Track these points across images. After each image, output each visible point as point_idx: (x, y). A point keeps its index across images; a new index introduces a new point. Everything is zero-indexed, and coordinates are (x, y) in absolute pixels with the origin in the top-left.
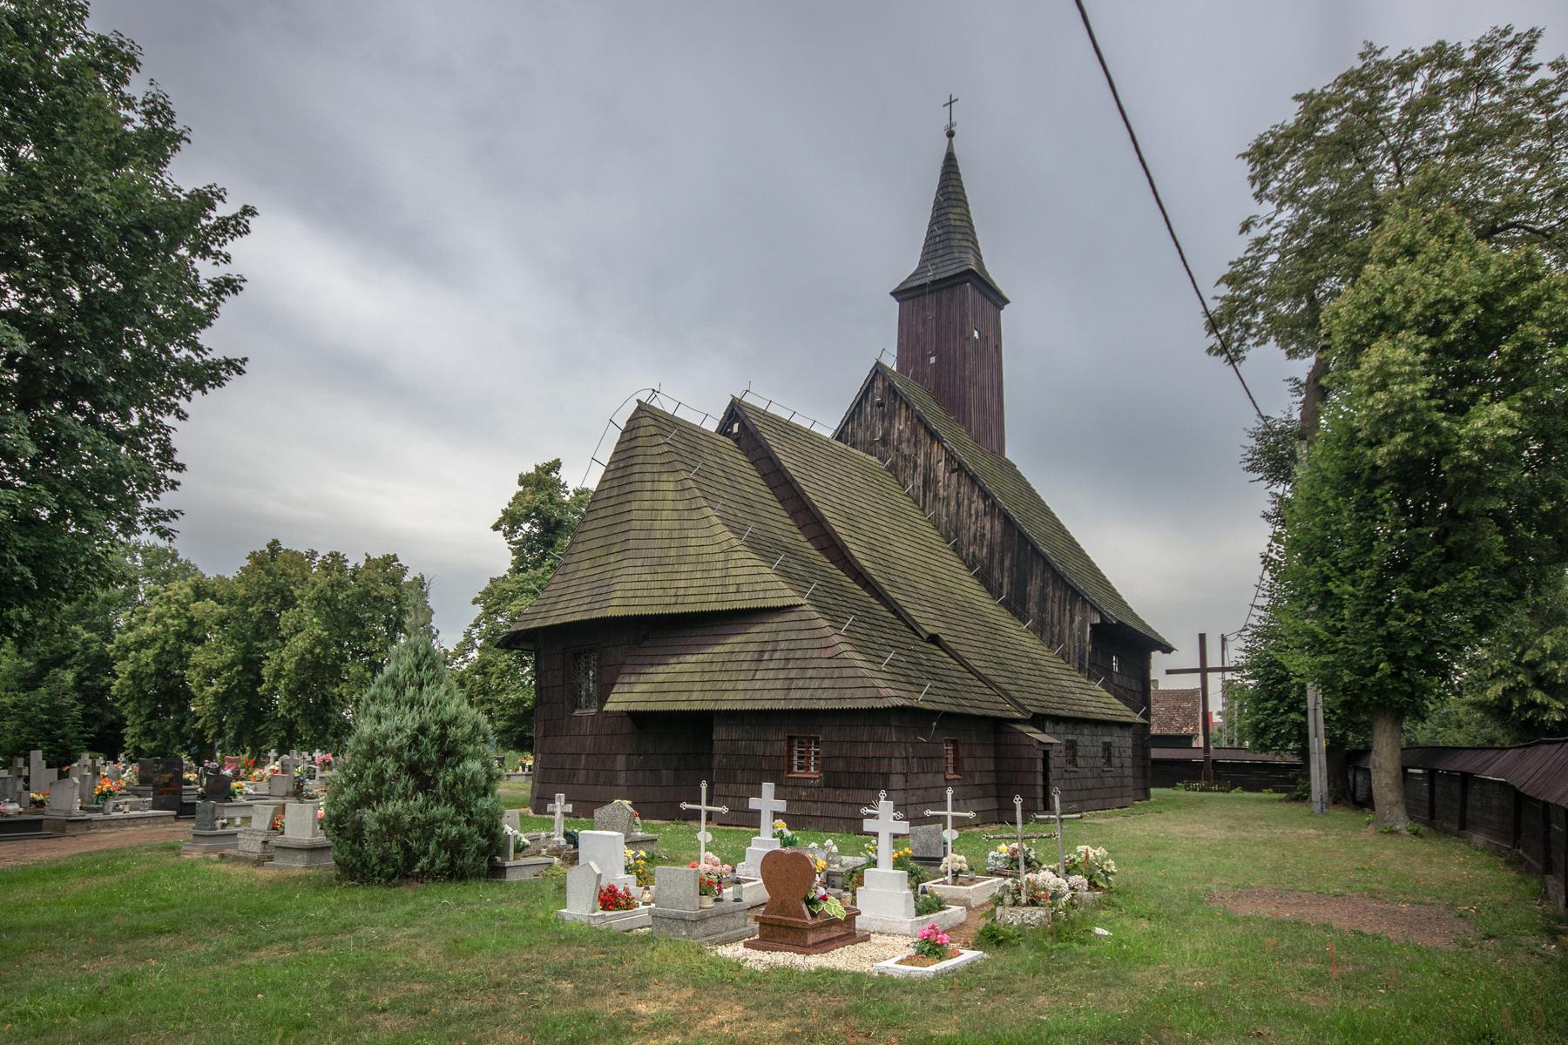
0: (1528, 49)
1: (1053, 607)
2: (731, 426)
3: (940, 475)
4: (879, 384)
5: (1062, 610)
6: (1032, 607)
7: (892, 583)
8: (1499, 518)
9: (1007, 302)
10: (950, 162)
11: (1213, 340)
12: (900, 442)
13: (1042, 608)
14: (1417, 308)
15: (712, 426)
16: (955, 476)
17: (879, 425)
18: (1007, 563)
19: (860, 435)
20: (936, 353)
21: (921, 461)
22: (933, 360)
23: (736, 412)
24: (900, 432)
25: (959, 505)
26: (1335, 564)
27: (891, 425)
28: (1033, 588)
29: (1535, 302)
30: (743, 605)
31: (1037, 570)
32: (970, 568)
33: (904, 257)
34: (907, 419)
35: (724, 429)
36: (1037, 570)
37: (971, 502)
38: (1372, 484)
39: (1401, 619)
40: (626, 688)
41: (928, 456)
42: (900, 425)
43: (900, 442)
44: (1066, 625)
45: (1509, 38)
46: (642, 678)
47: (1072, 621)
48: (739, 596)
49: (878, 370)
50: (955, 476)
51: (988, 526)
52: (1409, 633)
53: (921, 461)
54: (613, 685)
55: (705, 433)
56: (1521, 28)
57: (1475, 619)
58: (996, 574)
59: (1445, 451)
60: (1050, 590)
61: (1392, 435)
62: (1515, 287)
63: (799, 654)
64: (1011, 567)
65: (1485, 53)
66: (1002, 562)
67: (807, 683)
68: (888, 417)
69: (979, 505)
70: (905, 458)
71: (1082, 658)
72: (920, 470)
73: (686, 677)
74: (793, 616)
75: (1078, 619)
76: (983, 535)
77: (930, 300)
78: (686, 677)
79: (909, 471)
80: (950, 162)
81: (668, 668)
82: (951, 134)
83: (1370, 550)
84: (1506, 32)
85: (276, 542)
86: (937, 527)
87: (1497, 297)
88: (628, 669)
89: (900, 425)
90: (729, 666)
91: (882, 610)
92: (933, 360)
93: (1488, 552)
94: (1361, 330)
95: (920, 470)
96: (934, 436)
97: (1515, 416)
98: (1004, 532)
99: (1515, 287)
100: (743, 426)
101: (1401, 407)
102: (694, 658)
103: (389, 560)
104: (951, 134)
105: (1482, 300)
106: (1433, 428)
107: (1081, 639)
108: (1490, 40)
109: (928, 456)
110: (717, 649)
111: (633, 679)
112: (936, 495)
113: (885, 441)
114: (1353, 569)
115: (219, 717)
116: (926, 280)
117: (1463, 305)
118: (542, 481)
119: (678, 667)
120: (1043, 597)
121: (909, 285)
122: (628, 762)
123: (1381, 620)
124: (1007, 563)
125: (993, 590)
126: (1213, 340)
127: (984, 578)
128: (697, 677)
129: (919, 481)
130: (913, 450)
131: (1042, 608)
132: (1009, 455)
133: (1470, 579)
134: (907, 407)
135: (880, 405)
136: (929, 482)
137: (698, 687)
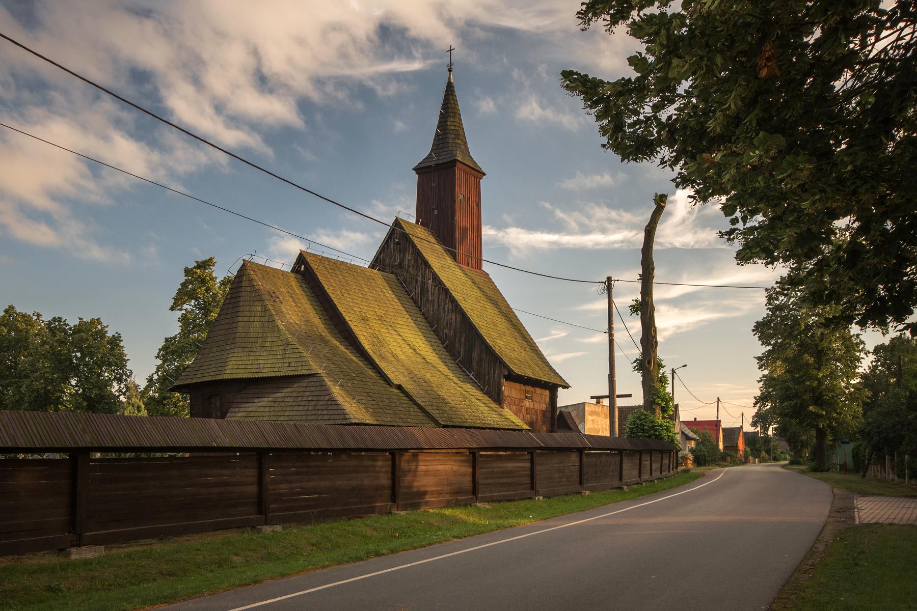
2: (300, 267)
3: (430, 287)
6: (474, 364)
7: (382, 357)
9: (484, 174)
10: (450, 87)
12: (409, 267)
15: (288, 269)
18: (463, 339)
19: (387, 261)
21: (419, 279)
22: (436, 212)
23: (302, 259)
24: (409, 261)
27: (404, 256)
28: (475, 355)
30: (291, 374)
33: (422, 149)
34: (412, 253)
35: (295, 270)
37: (445, 304)
40: (233, 414)
41: (423, 276)
43: (409, 267)
46: (242, 409)
48: (290, 369)
49: (397, 223)
53: (419, 279)
54: (227, 413)
55: (283, 273)
58: (457, 345)
60: (484, 356)
67: (316, 412)
68: (403, 251)
72: (419, 284)
73: (262, 409)
74: (314, 379)
75: (497, 372)
76: (451, 323)
78: (262, 409)
79: (413, 284)
80: (450, 87)
81: (254, 405)
85: (12, 307)
88: (235, 405)
89: (409, 257)
90: (282, 404)
91: (370, 372)
95: (419, 284)
102: (266, 400)
103: (95, 322)
104: (450, 70)
109: (423, 276)
110: (278, 395)
111: (237, 410)
112: (427, 299)
113: (401, 265)
115: (868, 464)
116: (432, 164)
118: (205, 265)
119: (259, 404)
121: (423, 165)
124: (463, 339)
128: (267, 409)
129: (419, 290)
132: (486, 267)
135: (398, 244)
136: (424, 291)
137: (267, 414)
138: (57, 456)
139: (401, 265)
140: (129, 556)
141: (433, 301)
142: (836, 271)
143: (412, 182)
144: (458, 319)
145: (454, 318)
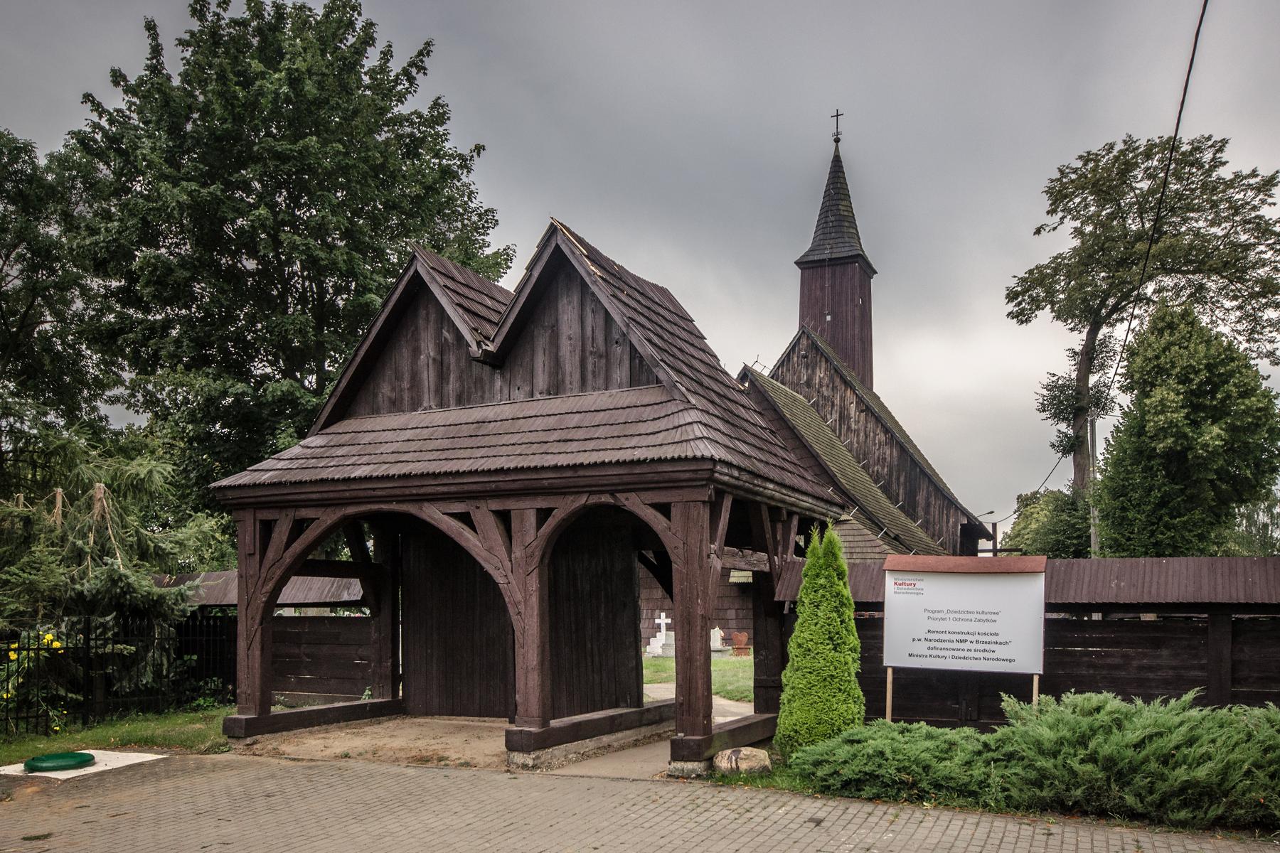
0: (1220, 150)
1: (934, 511)
4: (804, 341)
5: (941, 513)
6: (920, 512)
8: (1211, 481)
10: (837, 160)
11: (1011, 307)
13: (927, 513)
14: (1178, 370)
16: (863, 415)
17: (804, 371)
18: (902, 479)
20: (832, 313)
21: (837, 401)
22: (829, 318)
25: (866, 436)
26: (1130, 501)
28: (921, 498)
29: (1231, 374)
31: (924, 485)
32: (876, 482)
34: (826, 370)
36: (924, 485)
37: (875, 435)
38: (1150, 458)
39: (1162, 533)
41: (843, 399)
42: (820, 374)
43: (821, 385)
44: (944, 524)
45: (1210, 143)
47: (948, 521)
50: (863, 415)
51: (888, 452)
52: (1167, 542)
53: (837, 401)
56: (1217, 137)
57: (1198, 535)
58: (894, 486)
59: (1190, 448)
61: (1165, 437)
62: (1223, 363)
63: (858, 550)
64: (905, 483)
65: (1197, 148)
66: (898, 479)
68: (812, 366)
69: (881, 437)
70: (824, 398)
71: (955, 547)
76: (884, 459)
77: (828, 272)
80: (837, 160)
82: (837, 141)
83: (1148, 495)
84: (1209, 138)
86: (850, 451)
87: (1215, 366)
89: (820, 374)
92: (829, 318)
93: (1206, 499)
94: (1149, 373)
96: (847, 384)
97: (1223, 433)
98: (899, 458)
99: (1223, 363)
100: (752, 383)
101: (1171, 424)
104: (837, 141)
105: (1209, 367)
106: (1185, 436)
107: (954, 534)
108: (1200, 142)
109: (843, 399)
112: (849, 428)
113: (809, 384)
114: (1139, 505)
117: (1200, 370)
120: (928, 505)
122: (737, 615)
123: (1152, 534)
124: (902, 479)
125: (894, 500)
126: (1011, 307)
127: (886, 489)
129: (836, 416)
130: (831, 393)
131: (927, 513)
133: (1197, 515)
134: (827, 361)
135: (805, 357)
136: (843, 417)
138: (44, 765)
139: (809, 384)
140: (1187, 618)
141: (858, 431)
142: (177, 425)
143: (794, 277)
144: (895, 454)
145: (890, 453)
